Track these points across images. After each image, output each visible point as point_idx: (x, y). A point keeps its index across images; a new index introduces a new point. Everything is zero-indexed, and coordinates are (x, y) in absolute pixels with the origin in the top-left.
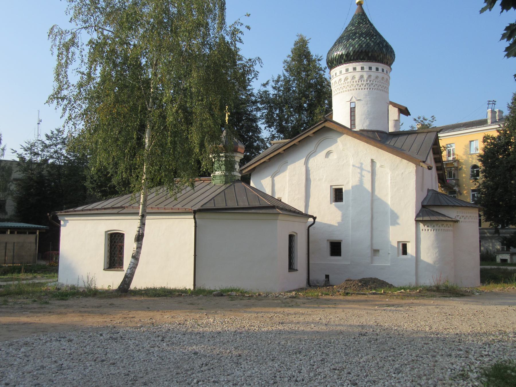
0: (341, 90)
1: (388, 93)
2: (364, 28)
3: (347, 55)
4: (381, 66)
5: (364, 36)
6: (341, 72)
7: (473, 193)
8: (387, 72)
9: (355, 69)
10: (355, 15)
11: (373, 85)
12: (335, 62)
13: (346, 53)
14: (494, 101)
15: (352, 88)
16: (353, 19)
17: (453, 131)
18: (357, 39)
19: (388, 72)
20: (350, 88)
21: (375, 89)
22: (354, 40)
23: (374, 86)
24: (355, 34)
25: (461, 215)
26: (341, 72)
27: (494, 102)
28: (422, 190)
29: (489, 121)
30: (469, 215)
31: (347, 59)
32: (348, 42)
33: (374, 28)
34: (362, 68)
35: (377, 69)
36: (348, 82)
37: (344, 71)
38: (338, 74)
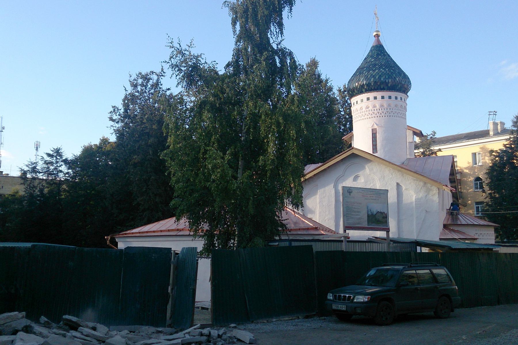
0: (363, 117)
1: (406, 119)
2: (382, 60)
3: (368, 85)
4: (399, 95)
5: (384, 68)
6: (362, 101)
7: (477, 206)
8: (405, 101)
9: (375, 98)
10: (373, 47)
11: (393, 113)
12: (356, 91)
13: (367, 83)
14: (494, 111)
15: (373, 115)
16: (371, 51)
17: (454, 143)
18: (377, 71)
19: (406, 100)
20: (372, 116)
21: (395, 116)
22: (374, 71)
23: (394, 114)
24: (375, 65)
25: (479, 232)
26: (362, 101)
27: (495, 113)
28: (443, 210)
29: (491, 133)
30: (486, 232)
31: (369, 88)
32: (369, 73)
33: (392, 59)
34: (383, 97)
35: (396, 98)
36: (369, 111)
37: (365, 99)
38: (359, 102)
